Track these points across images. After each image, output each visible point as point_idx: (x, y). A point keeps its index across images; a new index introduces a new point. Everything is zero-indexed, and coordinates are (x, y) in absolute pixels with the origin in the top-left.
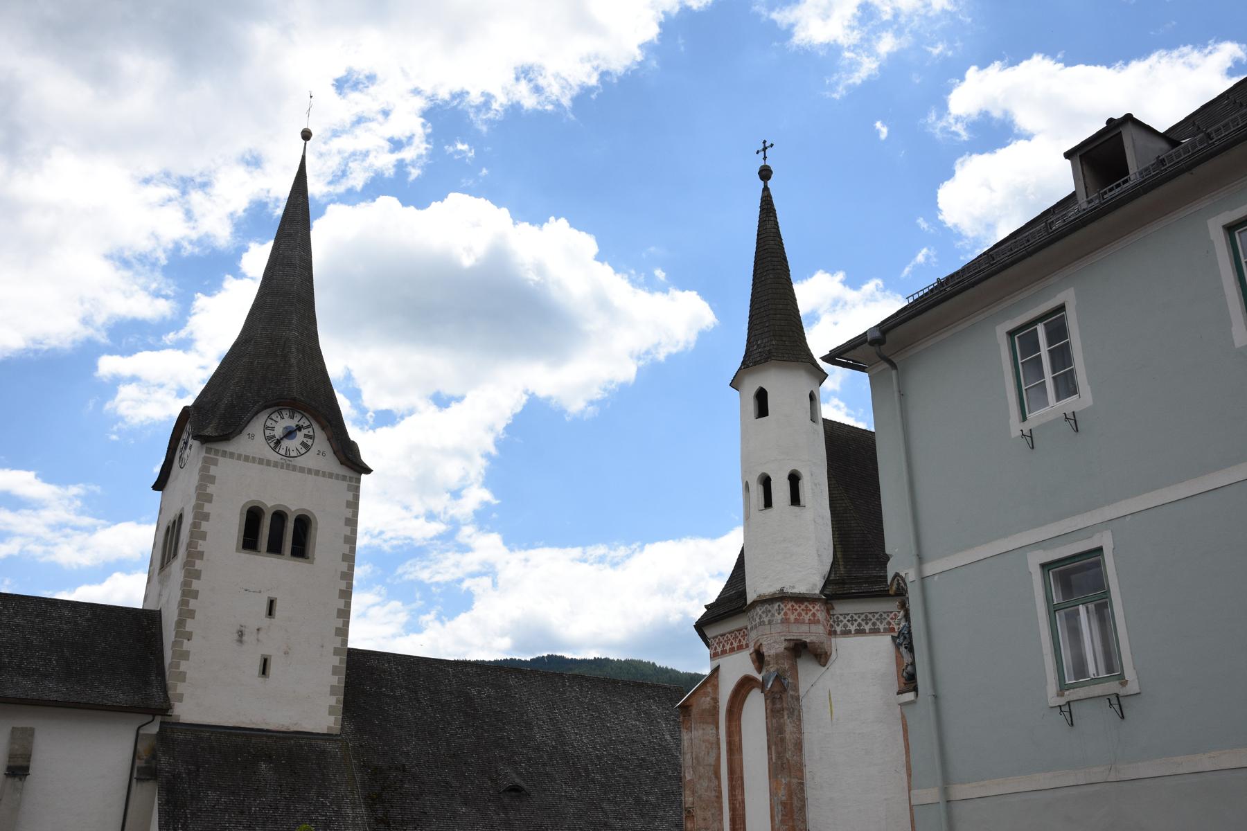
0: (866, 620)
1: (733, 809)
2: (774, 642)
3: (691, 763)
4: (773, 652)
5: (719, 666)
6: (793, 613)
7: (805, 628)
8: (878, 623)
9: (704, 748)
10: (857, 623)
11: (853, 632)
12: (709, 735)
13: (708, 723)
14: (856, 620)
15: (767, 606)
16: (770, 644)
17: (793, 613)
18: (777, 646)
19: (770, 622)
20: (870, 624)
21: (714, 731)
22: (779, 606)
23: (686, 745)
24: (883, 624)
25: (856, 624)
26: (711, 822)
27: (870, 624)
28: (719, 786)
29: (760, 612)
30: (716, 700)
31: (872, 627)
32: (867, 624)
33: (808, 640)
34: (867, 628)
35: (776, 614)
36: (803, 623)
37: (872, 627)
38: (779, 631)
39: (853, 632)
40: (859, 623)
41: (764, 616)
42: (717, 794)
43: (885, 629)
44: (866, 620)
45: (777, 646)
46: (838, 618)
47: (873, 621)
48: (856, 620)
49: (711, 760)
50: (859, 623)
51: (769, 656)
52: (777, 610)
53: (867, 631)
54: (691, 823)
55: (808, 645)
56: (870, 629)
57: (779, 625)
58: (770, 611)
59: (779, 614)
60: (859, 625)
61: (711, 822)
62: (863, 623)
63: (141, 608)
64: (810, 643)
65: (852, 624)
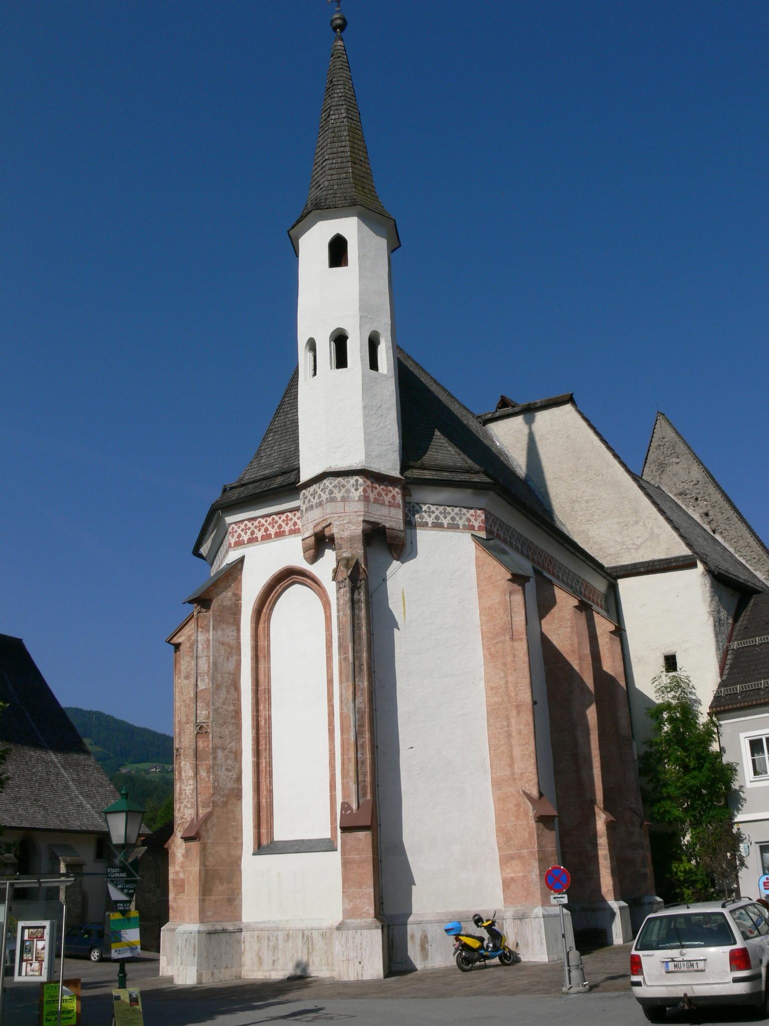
0: (445, 513)
1: (257, 727)
2: (349, 523)
3: (206, 669)
4: (346, 534)
5: (244, 557)
6: (373, 492)
7: (385, 511)
8: (457, 518)
9: (223, 652)
10: (435, 515)
11: (430, 525)
12: (228, 637)
13: (228, 623)
14: (433, 512)
15: (340, 479)
16: (343, 525)
17: (373, 492)
18: (353, 528)
19: (344, 499)
20: (449, 518)
21: (235, 633)
22: (357, 480)
23: (364, 628)
24: (463, 520)
25: (433, 516)
26: (228, 741)
27: (449, 518)
28: (239, 699)
29: (331, 487)
30: (238, 597)
31: (450, 521)
32: (445, 517)
33: (387, 525)
34: (446, 522)
35: (353, 490)
36: (383, 504)
37: (450, 521)
38: (357, 510)
39: (430, 525)
40: (437, 515)
41: (335, 491)
42: (235, 708)
43: (464, 525)
44: (445, 513)
45: (353, 528)
46: (413, 507)
47: (451, 515)
48: (433, 512)
49: (231, 666)
50: (437, 515)
51: (341, 538)
52: (353, 485)
53: (446, 526)
54: (203, 742)
55: (387, 531)
56: (448, 524)
57: (357, 502)
58: (344, 486)
59: (357, 490)
60: (437, 518)
61: (228, 741)
62: (441, 516)
63: (138, 929)
64: (389, 529)
65: (430, 516)
